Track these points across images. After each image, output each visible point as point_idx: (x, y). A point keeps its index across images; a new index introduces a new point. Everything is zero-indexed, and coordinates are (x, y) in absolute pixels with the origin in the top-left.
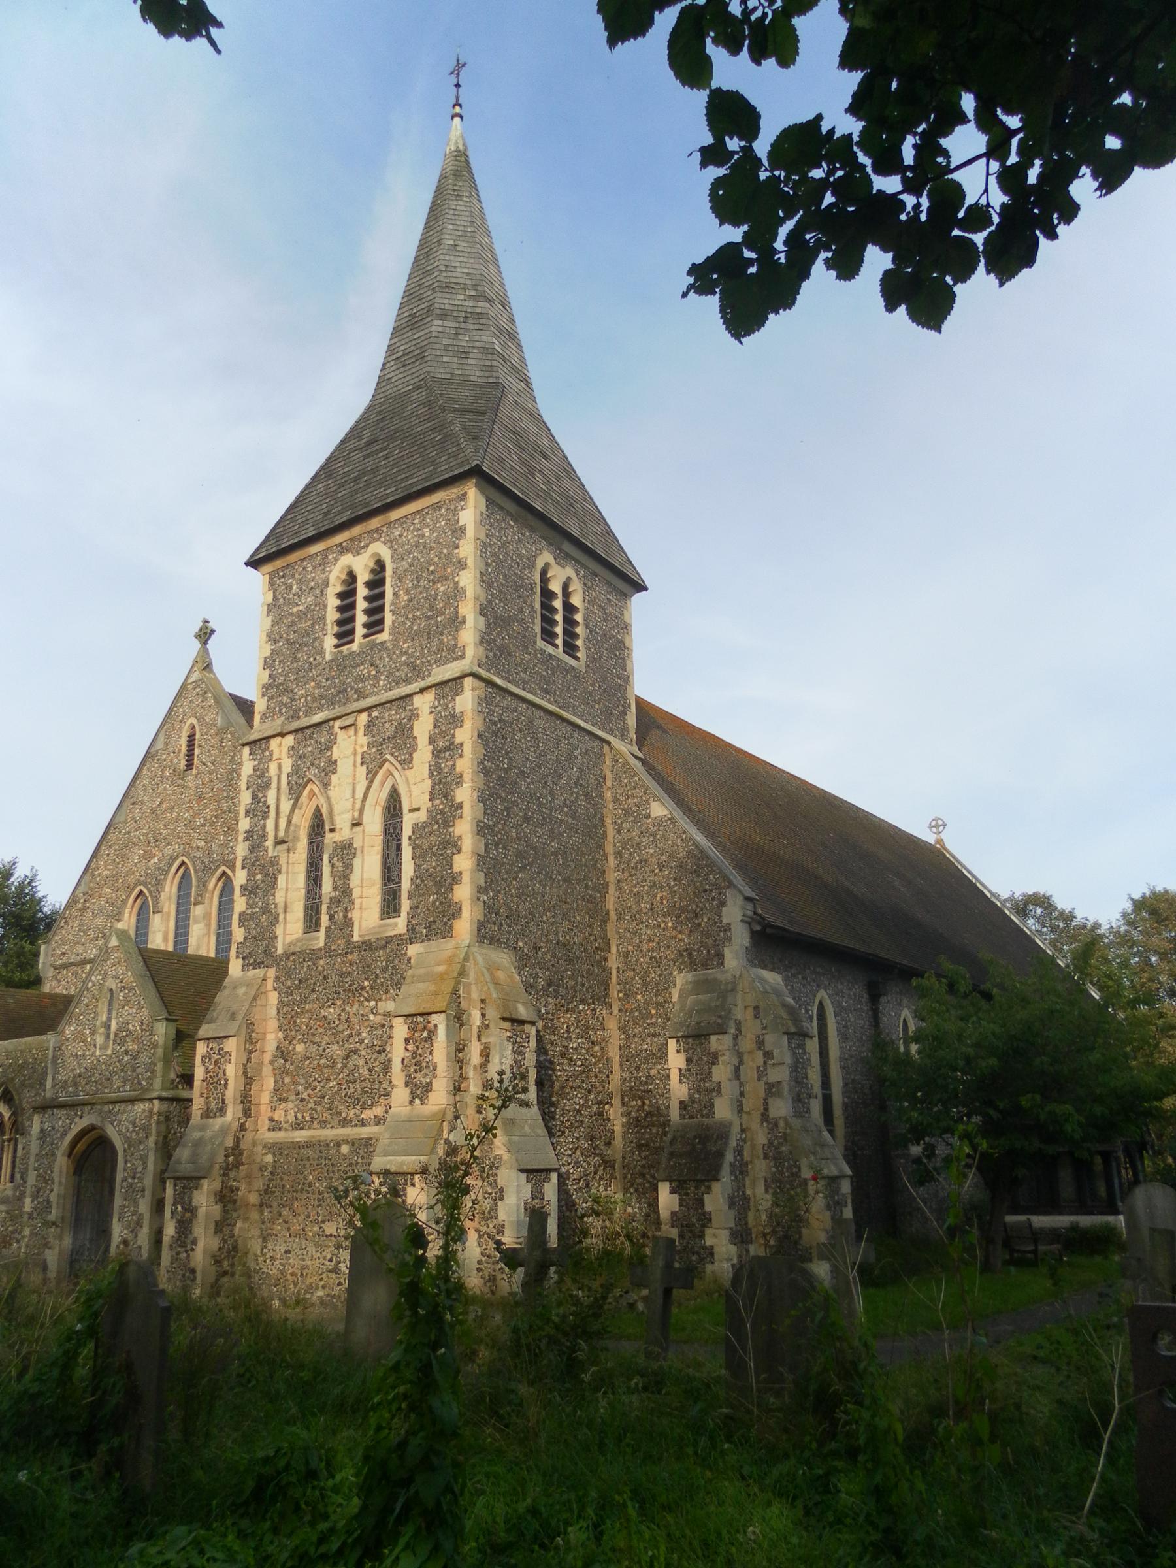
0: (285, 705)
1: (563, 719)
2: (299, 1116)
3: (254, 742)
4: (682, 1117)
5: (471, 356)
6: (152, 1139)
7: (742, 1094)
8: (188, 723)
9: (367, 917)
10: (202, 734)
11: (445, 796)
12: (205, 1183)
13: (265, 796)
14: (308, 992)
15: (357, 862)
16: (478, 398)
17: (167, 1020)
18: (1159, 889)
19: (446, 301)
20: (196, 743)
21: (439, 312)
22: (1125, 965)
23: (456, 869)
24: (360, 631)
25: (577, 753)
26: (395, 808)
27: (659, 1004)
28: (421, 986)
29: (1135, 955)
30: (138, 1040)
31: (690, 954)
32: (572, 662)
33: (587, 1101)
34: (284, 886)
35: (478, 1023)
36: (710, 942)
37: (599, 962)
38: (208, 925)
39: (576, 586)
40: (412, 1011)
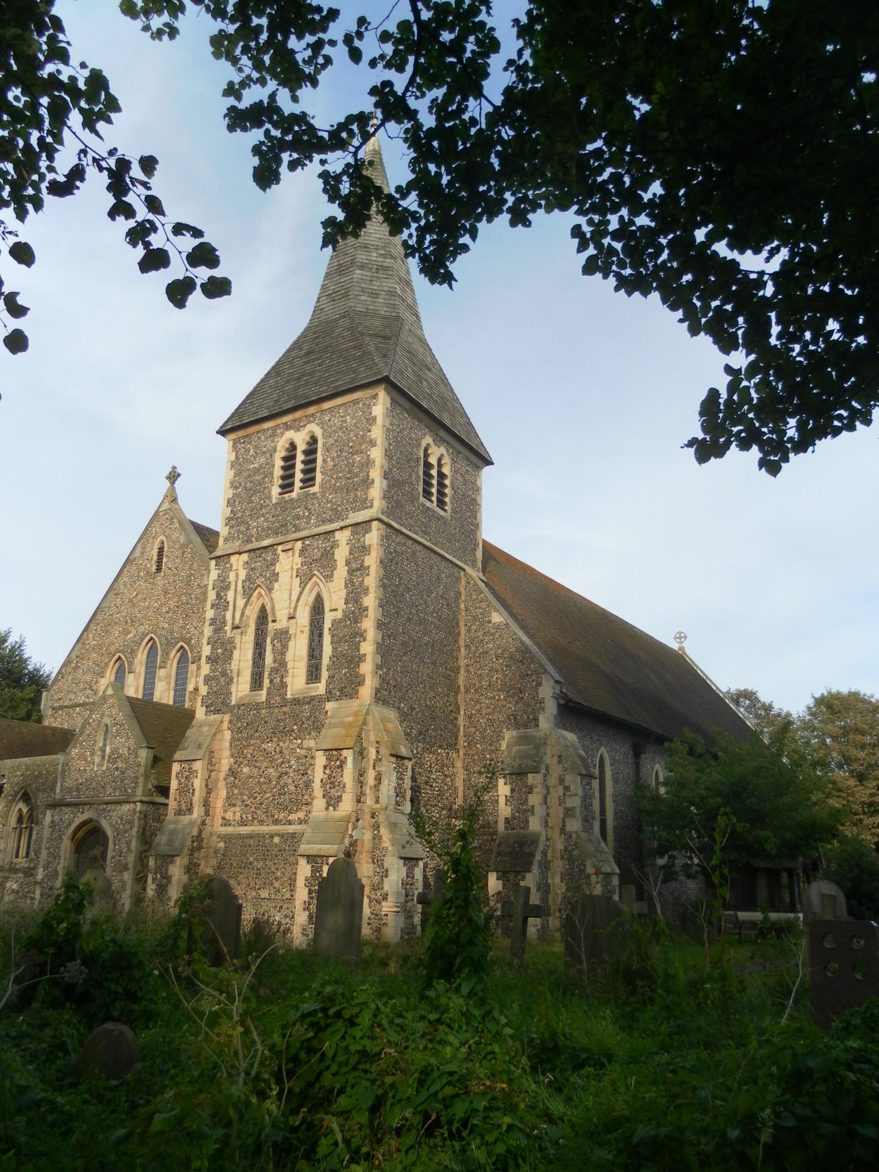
0: (242, 532)
1: (435, 553)
2: (244, 816)
3: (219, 557)
4: (506, 828)
5: (381, 296)
6: (135, 830)
7: (548, 815)
8: (159, 539)
9: (297, 682)
10: (173, 549)
11: (356, 602)
12: (178, 860)
13: (226, 595)
14: (252, 731)
15: (291, 644)
16: (385, 327)
17: (148, 747)
18: (834, 691)
19: (364, 257)
20: (165, 554)
21: (359, 264)
22: (808, 743)
23: (362, 652)
24: (298, 484)
25: (443, 576)
26: (319, 608)
27: (492, 751)
28: (335, 730)
29: (815, 737)
30: (126, 761)
31: (515, 718)
32: (442, 513)
33: (441, 815)
34: (238, 658)
35: (374, 757)
36: (530, 710)
37: (452, 721)
38: (169, 684)
39: (446, 460)
40: (330, 747)
